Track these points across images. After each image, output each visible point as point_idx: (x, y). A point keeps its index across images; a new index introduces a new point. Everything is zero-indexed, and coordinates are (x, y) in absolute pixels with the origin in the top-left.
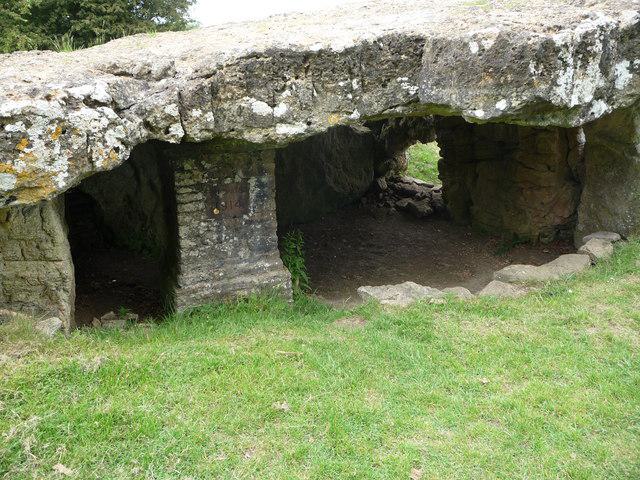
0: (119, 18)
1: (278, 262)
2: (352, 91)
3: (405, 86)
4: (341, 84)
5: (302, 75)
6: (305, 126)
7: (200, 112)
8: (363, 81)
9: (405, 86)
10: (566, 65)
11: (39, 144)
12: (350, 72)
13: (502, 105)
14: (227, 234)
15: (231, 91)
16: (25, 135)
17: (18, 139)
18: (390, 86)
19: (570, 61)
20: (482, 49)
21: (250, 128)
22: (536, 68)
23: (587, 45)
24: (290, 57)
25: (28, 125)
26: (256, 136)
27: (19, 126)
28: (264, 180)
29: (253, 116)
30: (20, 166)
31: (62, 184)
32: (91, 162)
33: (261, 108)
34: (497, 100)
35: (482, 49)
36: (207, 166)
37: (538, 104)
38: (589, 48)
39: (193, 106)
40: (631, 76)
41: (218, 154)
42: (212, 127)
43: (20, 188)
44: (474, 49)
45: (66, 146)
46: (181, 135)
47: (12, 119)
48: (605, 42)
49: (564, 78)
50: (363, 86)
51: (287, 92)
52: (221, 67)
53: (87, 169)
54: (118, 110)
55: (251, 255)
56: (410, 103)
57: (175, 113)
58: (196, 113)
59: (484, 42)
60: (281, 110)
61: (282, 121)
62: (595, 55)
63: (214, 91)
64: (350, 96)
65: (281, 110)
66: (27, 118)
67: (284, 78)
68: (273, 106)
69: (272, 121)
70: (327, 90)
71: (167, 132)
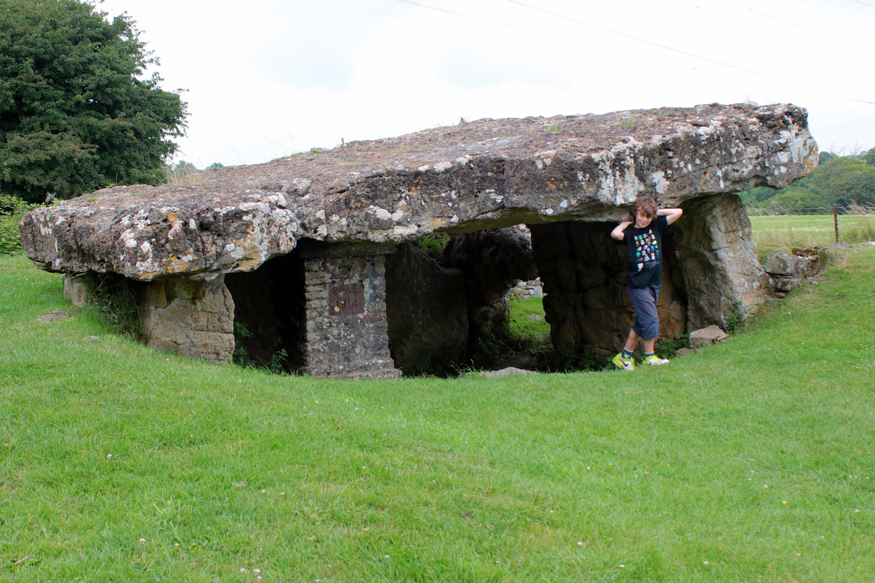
0: (315, 152)
1: (390, 361)
2: (451, 200)
3: (493, 196)
4: (443, 195)
5: (413, 188)
6: (416, 228)
7: (338, 218)
8: (459, 192)
9: (493, 196)
10: (606, 174)
12: (449, 186)
13: (564, 204)
14: (345, 331)
15: (359, 201)
16: (252, 223)
17: (248, 224)
18: (481, 196)
19: (610, 171)
20: (545, 165)
22: (584, 177)
23: (621, 160)
24: (404, 176)
25: (254, 216)
26: (378, 237)
28: (376, 282)
31: (263, 259)
32: (278, 246)
33: (382, 214)
34: (560, 201)
35: (545, 165)
36: (332, 268)
37: (590, 202)
38: (622, 162)
39: (333, 213)
40: (668, 183)
41: (348, 252)
42: (345, 229)
44: (540, 166)
45: (269, 233)
46: (325, 234)
47: (247, 213)
48: (635, 158)
49: (607, 183)
50: (459, 196)
51: (403, 202)
52: (352, 184)
53: (275, 251)
55: (366, 352)
56: (498, 209)
57: (323, 217)
58: (335, 218)
59: (545, 160)
60: (398, 215)
61: (399, 223)
62: (628, 167)
63: (347, 203)
64: (450, 204)
65: (398, 215)
67: (400, 191)
68: (392, 212)
69: (388, 225)
70: (432, 199)
71: (316, 232)
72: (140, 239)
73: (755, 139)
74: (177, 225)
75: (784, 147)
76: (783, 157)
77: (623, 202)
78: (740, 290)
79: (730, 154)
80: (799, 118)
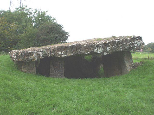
2: (71, 51)
3: (79, 51)
11: (35, 55)
13: (88, 52)
21: (59, 56)
26: (59, 57)
27: (33, 53)
29: (59, 54)
30: (33, 57)
33: (60, 53)
43: (32, 59)
48: (102, 45)
54: (43, 52)
58: (52, 53)
61: (63, 55)
62: (100, 47)
65: (62, 53)
66: (34, 52)
69: (61, 55)
72: (14, 56)
73: (129, 42)
74: (20, 54)
75: (136, 43)
76: (136, 45)
77: (147, 57)
78: (128, 68)
79: (123, 45)
80: (140, 38)
